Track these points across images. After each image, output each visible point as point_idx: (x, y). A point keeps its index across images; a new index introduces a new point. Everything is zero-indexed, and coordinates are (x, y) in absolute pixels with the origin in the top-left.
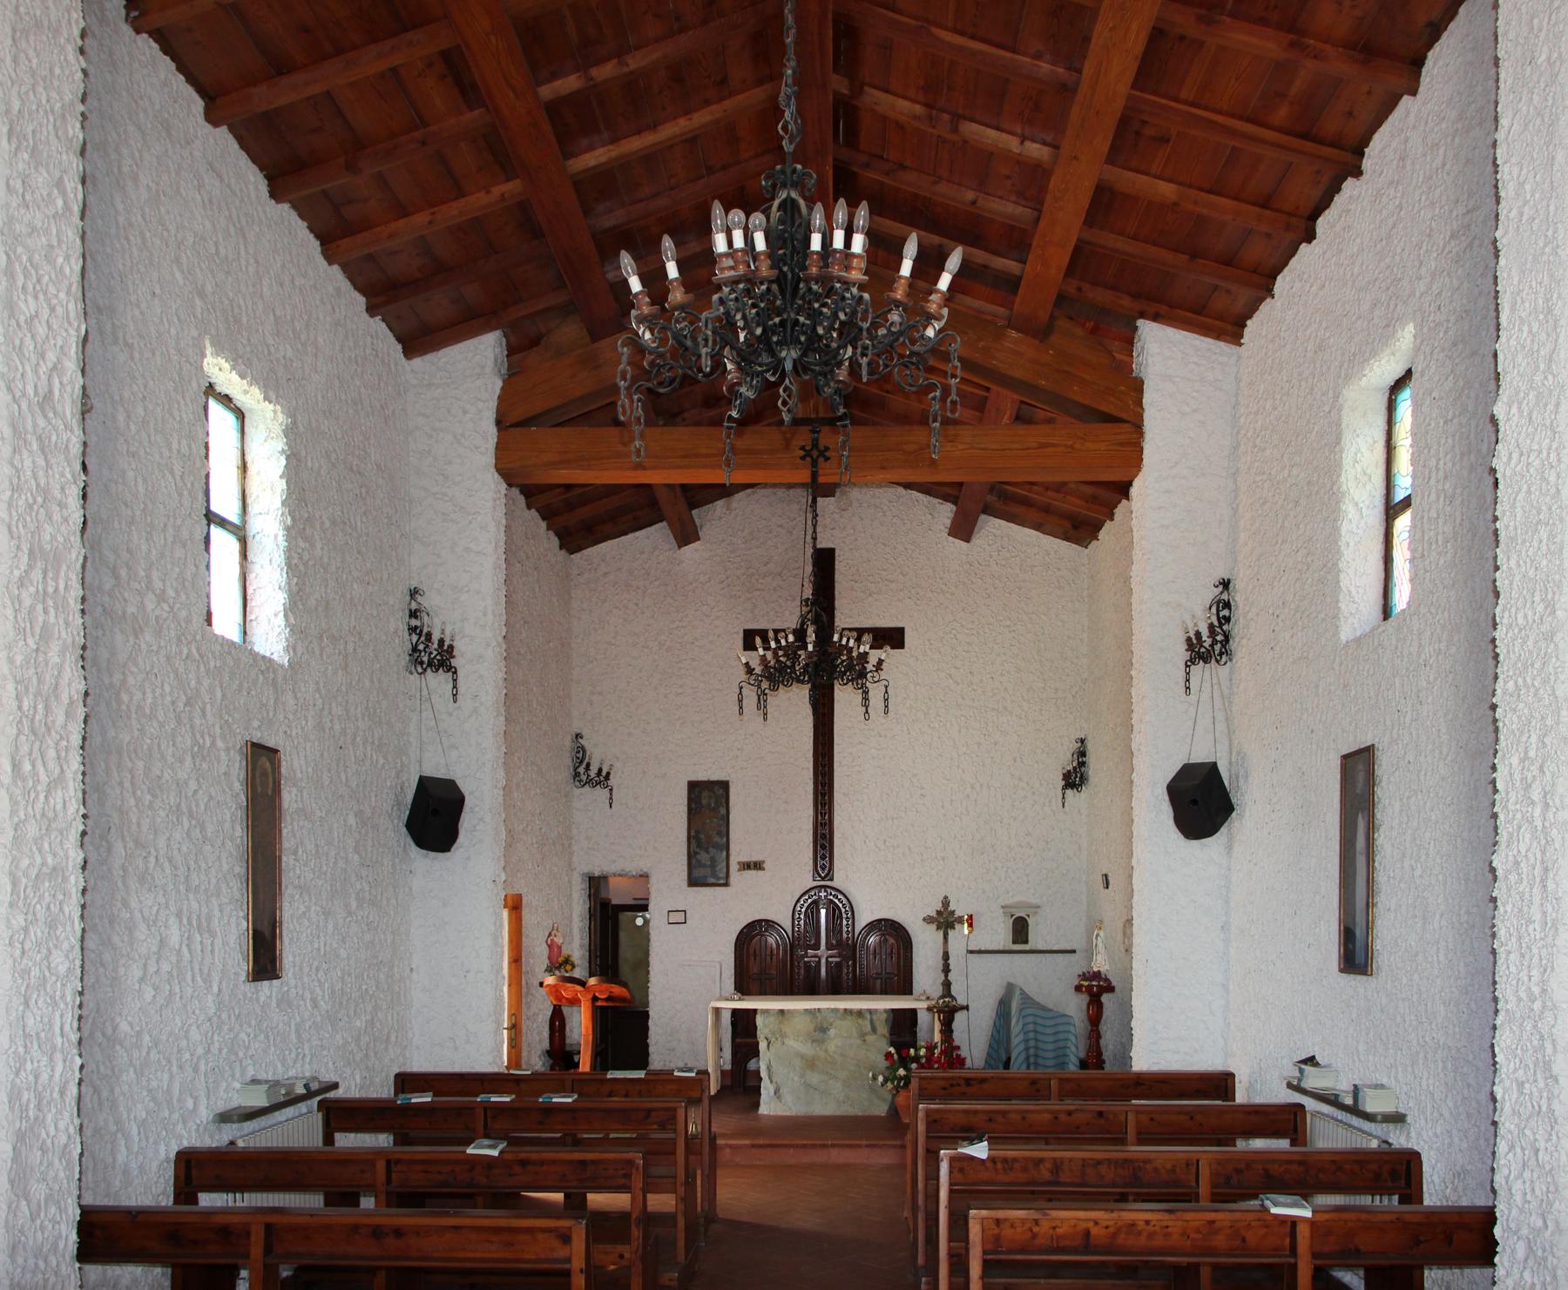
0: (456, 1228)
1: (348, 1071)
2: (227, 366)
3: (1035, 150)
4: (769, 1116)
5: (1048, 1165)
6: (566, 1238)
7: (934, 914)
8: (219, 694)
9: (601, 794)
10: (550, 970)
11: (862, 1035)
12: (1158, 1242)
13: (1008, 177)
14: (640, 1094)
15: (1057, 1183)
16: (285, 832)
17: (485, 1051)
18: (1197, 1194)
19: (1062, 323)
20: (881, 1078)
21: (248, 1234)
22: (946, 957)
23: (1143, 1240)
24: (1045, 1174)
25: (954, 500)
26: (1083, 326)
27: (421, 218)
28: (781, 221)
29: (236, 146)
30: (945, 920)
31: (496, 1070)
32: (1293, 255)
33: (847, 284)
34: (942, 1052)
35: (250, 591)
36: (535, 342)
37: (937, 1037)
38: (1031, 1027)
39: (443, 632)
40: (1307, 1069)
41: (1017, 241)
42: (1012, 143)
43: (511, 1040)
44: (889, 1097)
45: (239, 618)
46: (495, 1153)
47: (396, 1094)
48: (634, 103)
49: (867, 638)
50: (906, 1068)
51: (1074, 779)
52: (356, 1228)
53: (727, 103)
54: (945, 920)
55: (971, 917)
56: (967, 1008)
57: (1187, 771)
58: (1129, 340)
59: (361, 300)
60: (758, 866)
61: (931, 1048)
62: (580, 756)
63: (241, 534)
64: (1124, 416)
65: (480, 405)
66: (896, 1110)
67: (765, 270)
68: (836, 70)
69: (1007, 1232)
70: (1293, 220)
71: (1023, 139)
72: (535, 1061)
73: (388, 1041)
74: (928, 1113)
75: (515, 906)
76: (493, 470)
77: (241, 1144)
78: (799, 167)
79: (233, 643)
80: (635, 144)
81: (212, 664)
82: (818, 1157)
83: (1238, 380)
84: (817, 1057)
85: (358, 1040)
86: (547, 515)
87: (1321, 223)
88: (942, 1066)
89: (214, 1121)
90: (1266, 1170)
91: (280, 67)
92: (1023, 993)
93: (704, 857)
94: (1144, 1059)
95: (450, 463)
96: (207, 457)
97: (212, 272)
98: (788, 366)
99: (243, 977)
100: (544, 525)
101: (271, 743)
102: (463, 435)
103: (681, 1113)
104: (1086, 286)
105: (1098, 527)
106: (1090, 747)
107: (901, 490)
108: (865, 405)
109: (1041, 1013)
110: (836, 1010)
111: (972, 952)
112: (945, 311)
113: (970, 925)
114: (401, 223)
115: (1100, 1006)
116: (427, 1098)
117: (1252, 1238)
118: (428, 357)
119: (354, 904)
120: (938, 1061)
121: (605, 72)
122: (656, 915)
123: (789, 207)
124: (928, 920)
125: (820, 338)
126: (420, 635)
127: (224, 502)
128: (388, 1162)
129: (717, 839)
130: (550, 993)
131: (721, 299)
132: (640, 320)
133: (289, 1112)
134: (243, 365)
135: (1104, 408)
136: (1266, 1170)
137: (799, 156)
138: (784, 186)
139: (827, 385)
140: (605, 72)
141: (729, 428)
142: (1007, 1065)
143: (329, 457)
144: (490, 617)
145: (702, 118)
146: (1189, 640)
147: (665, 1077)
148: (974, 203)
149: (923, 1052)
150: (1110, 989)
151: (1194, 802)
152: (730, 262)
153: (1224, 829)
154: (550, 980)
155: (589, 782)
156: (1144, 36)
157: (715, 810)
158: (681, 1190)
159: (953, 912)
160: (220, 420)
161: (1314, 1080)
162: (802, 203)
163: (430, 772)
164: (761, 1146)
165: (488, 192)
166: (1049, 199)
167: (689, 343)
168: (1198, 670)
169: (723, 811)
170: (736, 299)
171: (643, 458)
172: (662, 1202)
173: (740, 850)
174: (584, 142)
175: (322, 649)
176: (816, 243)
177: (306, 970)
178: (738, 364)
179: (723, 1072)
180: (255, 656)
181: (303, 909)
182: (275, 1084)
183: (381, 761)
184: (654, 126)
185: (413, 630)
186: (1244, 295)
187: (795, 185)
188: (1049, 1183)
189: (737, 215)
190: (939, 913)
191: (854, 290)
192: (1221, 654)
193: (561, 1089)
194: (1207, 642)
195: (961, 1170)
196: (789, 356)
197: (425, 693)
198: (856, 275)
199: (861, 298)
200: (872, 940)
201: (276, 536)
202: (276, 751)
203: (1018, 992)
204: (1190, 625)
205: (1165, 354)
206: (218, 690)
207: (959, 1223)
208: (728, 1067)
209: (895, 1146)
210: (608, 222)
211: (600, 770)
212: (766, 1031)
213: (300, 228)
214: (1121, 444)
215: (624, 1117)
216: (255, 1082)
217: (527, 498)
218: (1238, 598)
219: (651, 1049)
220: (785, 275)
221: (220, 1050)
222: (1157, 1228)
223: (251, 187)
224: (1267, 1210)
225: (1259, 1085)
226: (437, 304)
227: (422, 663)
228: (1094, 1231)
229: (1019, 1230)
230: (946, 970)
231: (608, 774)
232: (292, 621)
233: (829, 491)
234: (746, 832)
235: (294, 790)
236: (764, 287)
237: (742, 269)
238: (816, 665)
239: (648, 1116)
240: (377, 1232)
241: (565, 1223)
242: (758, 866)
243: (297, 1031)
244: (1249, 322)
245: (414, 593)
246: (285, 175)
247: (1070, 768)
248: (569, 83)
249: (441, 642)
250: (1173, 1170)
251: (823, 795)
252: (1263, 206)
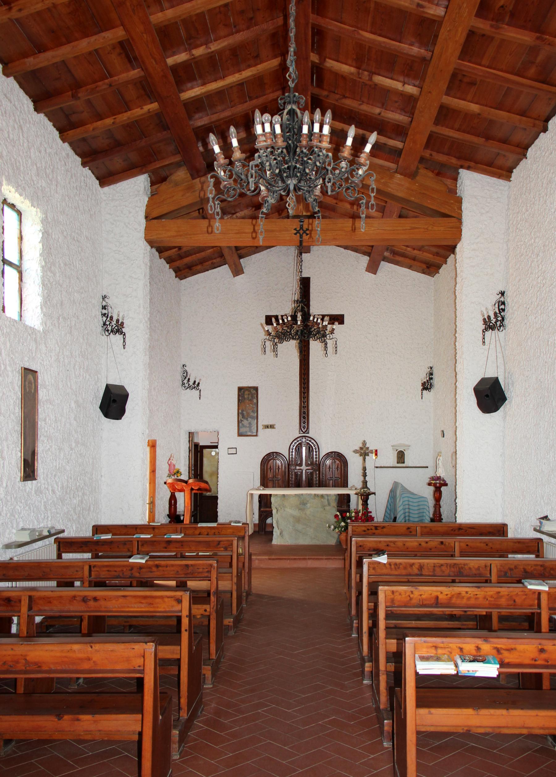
0: (124, 596)
1: (70, 524)
2: (13, 190)
3: (410, 89)
4: (277, 545)
5: (417, 566)
6: (179, 601)
7: (358, 449)
8: (8, 345)
9: (195, 392)
10: (169, 476)
11: (323, 506)
12: (472, 602)
13: (396, 102)
14: (214, 534)
15: (421, 575)
16: (40, 410)
17: (138, 516)
18: (491, 580)
19: (422, 171)
20: (332, 527)
21: (20, 601)
22: (364, 469)
23: (464, 601)
24: (415, 570)
25: (369, 254)
26: (433, 172)
27: (109, 121)
28: (288, 120)
29: (18, 86)
30: (364, 452)
31: (142, 523)
32: (537, 139)
33: (320, 149)
34: (362, 514)
35: (24, 296)
36: (164, 179)
37: (360, 507)
38: (407, 503)
39: (118, 315)
40: (544, 522)
41: (400, 131)
42: (398, 85)
43: (150, 509)
44: (336, 536)
45: (18, 309)
46: (143, 561)
47: (93, 535)
48: (213, 66)
49: (327, 318)
50: (344, 522)
51: (427, 386)
52: (74, 597)
53: (259, 66)
54: (364, 452)
55: (376, 451)
56: (374, 493)
57: (483, 381)
58: (455, 179)
59: (79, 160)
60: (272, 427)
61: (357, 512)
62: (185, 375)
63: (19, 269)
64: (453, 214)
65: (137, 209)
66: (340, 542)
67: (280, 142)
68: (313, 52)
69: (397, 597)
70: (537, 122)
71: (404, 83)
72: (162, 518)
73: (89, 510)
74: (357, 543)
75: (153, 445)
76: (143, 240)
77: (15, 559)
78: (297, 94)
79: (15, 321)
80: (213, 86)
81: (5, 331)
82: (302, 564)
83: (509, 197)
84: (301, 518)
85: (75, 509)
86: (169, 261)
87: (551, 124)
88: (363, 521)
89: (3, 548)
90: (524, 569)
91: (41, 49)
92: (402, 486)
93: (245, 422)
94: (465, 516)
95: (122, 236)
96: (3, 233)
97: (6, 146)
98: (292, 188)
99: (19, 479)
100: (168, 266)
101: (33, 368)
102: (129, 223)
103: (235, 543)
104: (434, 154)
105: (439, 267)
106: (435, 371)
107: (342, 249)
108: (327, 209)
109: (412, 496)
110: (310, 495)
111: (377, 467)
112: (368, 162)
113: (376, 455)
114: (99, 123)
115: (440, 493)
116: (109, 536)
117: (518, 601)
118: (112, 187)
119: (74, 445)
120: (361, 518)
121: (199, 52)
122: (222, 450)
123: (292, 113)
124: (355, 452)
125: (307, 174)
126: (107, 317)
127: (12, 255)
128: (90, 566)
129: (252, 414)
130: (169, 487)
131: (259, 156)
132: (220, 166)
133: (40, 543)
134: (20, 189)
135: (443, 210)
136: (524, 569)
137: (296, 89)
138: (289, 103)
139: (310, 197)
140: (199, 52)
141: (262, 217)
142: (395, 519)
143: (63, 233)
144: (142, 309)
145: (247, 73)
146: (484, 319)
147: (227, 526)
148: (379, 114)
149: (353, 514)
150: (446, 485)
151: (487, 396)
152: (264, 139)
153: (502, 409)
154: (170, 481)
155: (189, 387)
156: (465, 35)
157: (251, 400)
158: (235, 580)
159: (368, 448)
160: (10, 215)
161: (548, 527)
162: (298, 111)
163: (111, 382)
164: (273, 559)
165: (142, 108)
166: (417, 111)
167: (243, 177)
168: (489, 333)
169: (255, 401)
170: (267, 156)
171: (221, 231)
172: (225, 585)
173: (264, 418)
174: (189, 85)
175: (59, 324)
176: (305, 129)
177: (50, 476)
178: (267, 187)
179: (255, 524)
180: (26, 327)
181: (48, 447)
182: (33, 530)
183: (88, 377)
184: (224, 77)
185: (104, 315)
186: (512, 157)
187: (294, 102)
188: (417, 575)
189: (267, 116)
190: (361, 448)
191: (324, 152)
192: (500, 326)
193: (176, 532)
194: (494, 321)
195: (374, 569)
196: (292, 183)
197: (109, 344)
198: (325, 144)
199: (328, 155)
200: (328, 462)
201: (37, 271)
202: (36, 372)
203: (400, 486)
204: (485, 313)
205: (472, 184)
206: (8, 342)
207: (374, 593)
208: (257, 522)
209: (340, 559)
210: (199, 123)
211: (195, 382)
212: (276, 505)
213: (49, 125)
214: (452, 228)
215: (207, 545)
216: (23, 529)
217: (159, 253)
218: (508, 300)
219: (219, 514)
220: (290, 145)
221: (6, 515)
222: (472, 595)
223: (25, 106)
224: (526, 587)
225: (520, 529)
226: (117, 161)
227: (108, 331)
228: (441, 597)
229: (403, 596)
230: (365, 475)
231: (199, 383)
232: (44, 310)
233: (308, 251)
234: (265, 414)
235: (45, 390)
236: (280, 151)
237: (269, 142)
238: (302, 331)
239: (219, 544)
240: (85, 600)
241: (179, 594)
242: (272, 427)
243: (45, 505)
244: (514, 170)
245: (104, 298)
246: (40, 101)
247: (425, 380)
248: (182, 57)
249: (118, 321)
250: (478, 569)
251: (304, 393)
252: (522, 115)
